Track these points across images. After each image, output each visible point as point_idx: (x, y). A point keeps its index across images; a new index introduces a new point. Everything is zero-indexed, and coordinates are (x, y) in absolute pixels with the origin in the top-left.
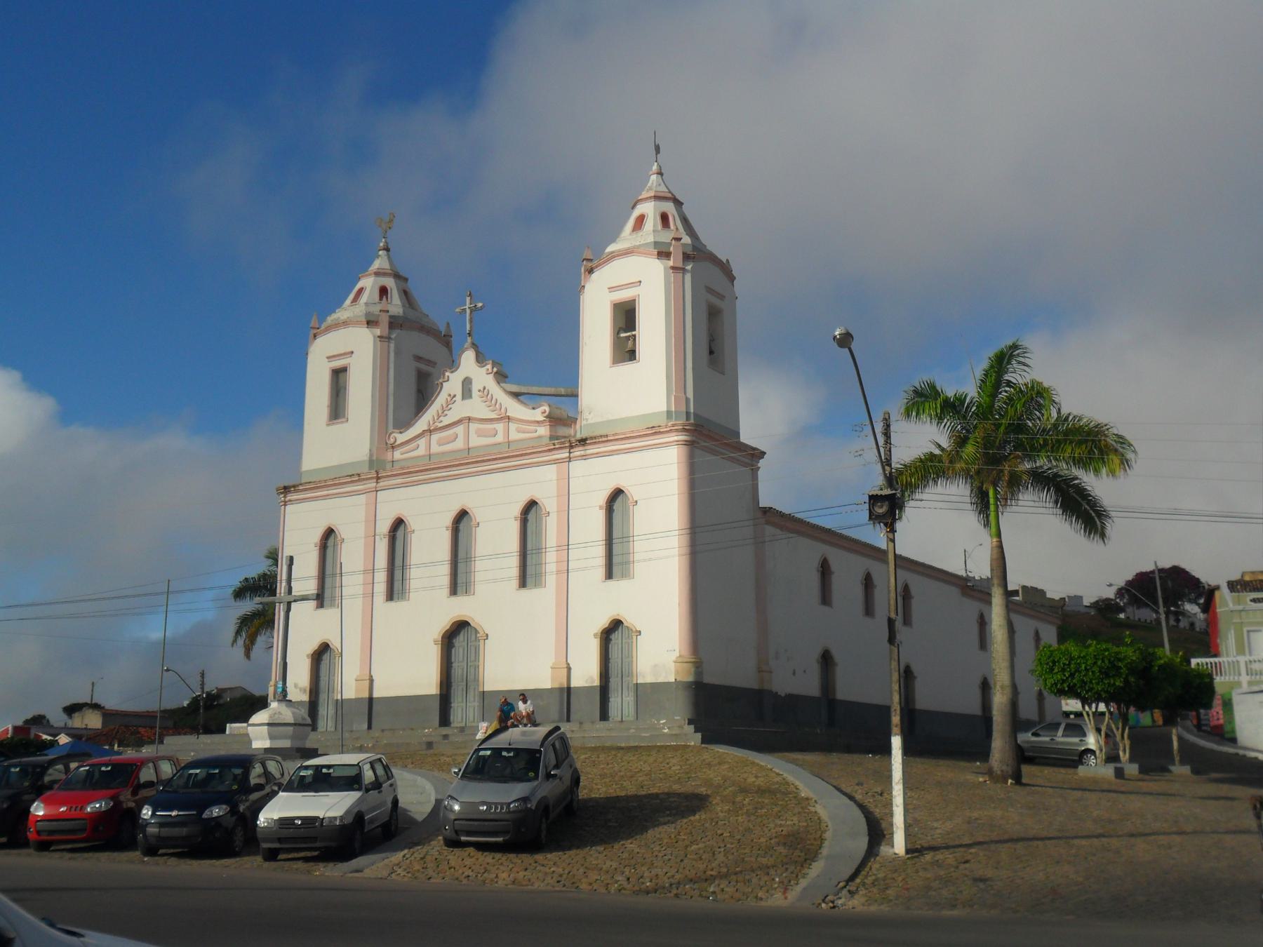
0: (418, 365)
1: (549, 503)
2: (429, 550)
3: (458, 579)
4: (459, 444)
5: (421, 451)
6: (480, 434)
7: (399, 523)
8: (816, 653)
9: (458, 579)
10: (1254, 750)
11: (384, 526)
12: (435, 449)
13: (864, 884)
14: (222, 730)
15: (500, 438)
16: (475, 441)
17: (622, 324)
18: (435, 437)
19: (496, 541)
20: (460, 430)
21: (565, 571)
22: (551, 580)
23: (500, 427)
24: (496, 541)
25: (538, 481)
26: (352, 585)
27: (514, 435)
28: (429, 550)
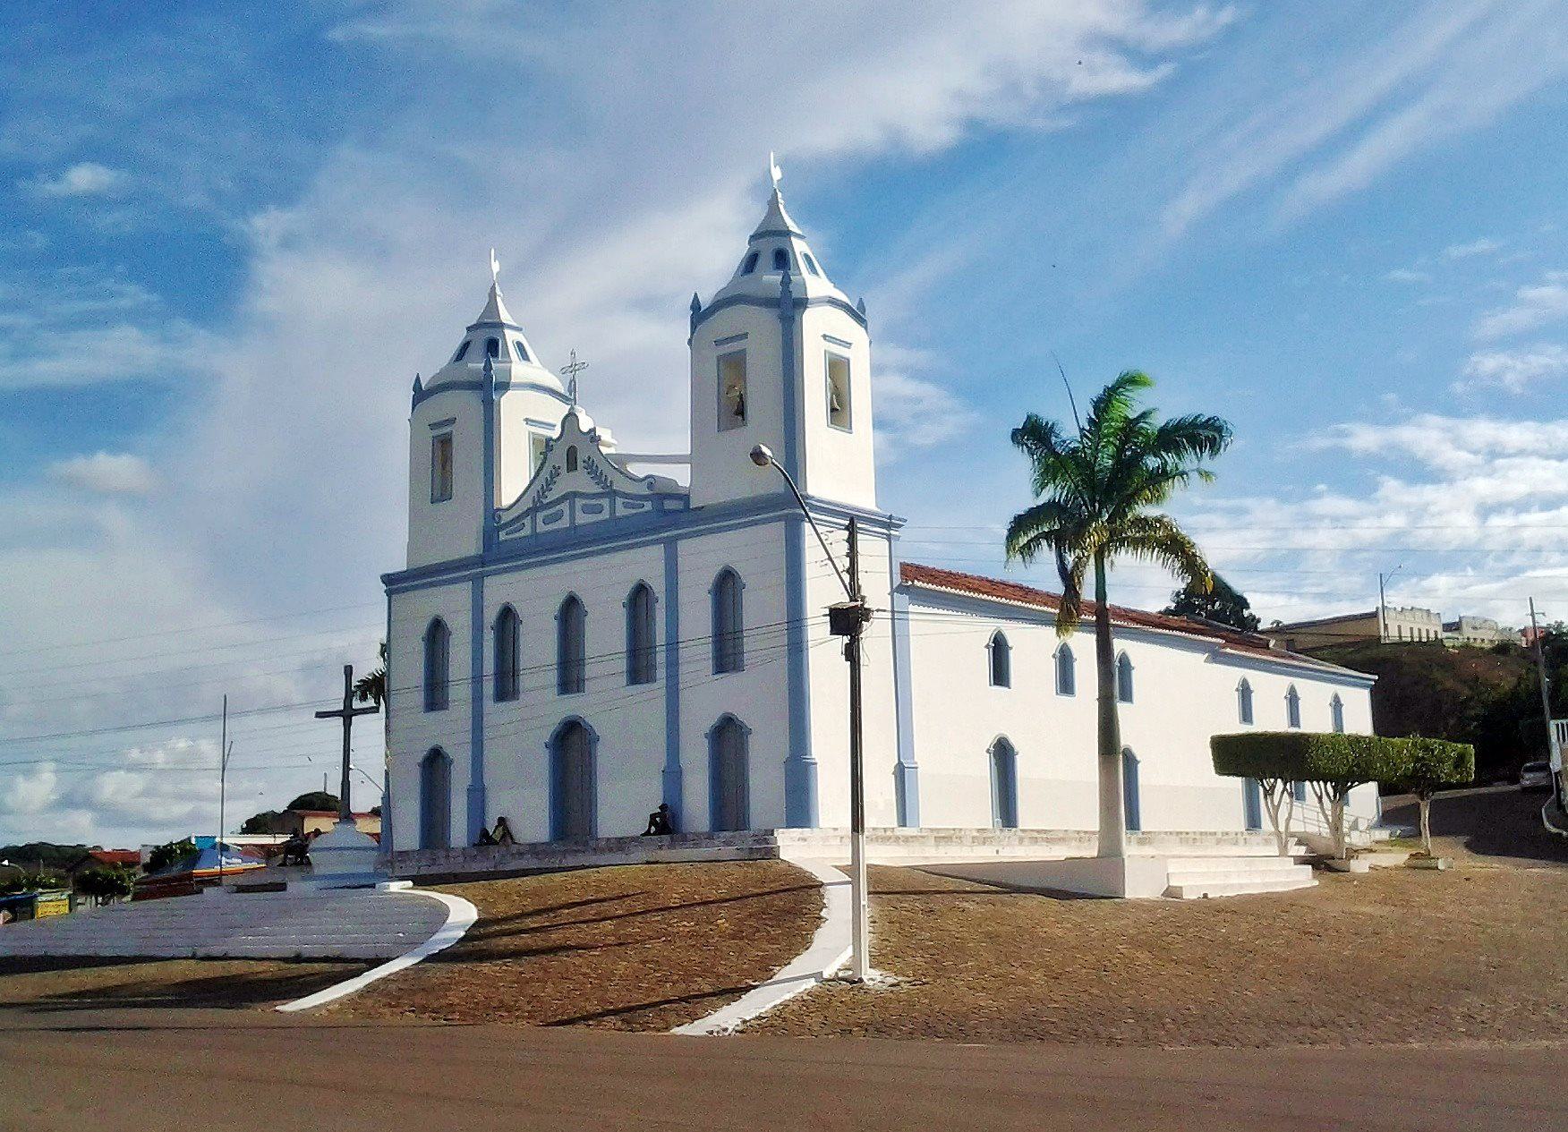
0: (533, 429)
1: (658, 587)
2: (538, 647)
3: (570, 677)
4: (564, 523)
5: (527, 531)
6: (586, 509)
7: (507, 614)
8: (989, 741)
9: (570, 677)
10: (673, 776)
11: (491, 616)
12: (542, 528)
13: (742, 950)
14: (201, 892)
15: (605, 515)
16: (582, 519)
17: (437, 494)
18: (540, 516)
19: (605, 636)
20: (565, 506)
21: (673, 665)
22: (661, 673)
23: (605, 502)
24: (605, 636)
25: (645, 563)
26: (459, 692)
27: (621, 511)
28: (538, 647)
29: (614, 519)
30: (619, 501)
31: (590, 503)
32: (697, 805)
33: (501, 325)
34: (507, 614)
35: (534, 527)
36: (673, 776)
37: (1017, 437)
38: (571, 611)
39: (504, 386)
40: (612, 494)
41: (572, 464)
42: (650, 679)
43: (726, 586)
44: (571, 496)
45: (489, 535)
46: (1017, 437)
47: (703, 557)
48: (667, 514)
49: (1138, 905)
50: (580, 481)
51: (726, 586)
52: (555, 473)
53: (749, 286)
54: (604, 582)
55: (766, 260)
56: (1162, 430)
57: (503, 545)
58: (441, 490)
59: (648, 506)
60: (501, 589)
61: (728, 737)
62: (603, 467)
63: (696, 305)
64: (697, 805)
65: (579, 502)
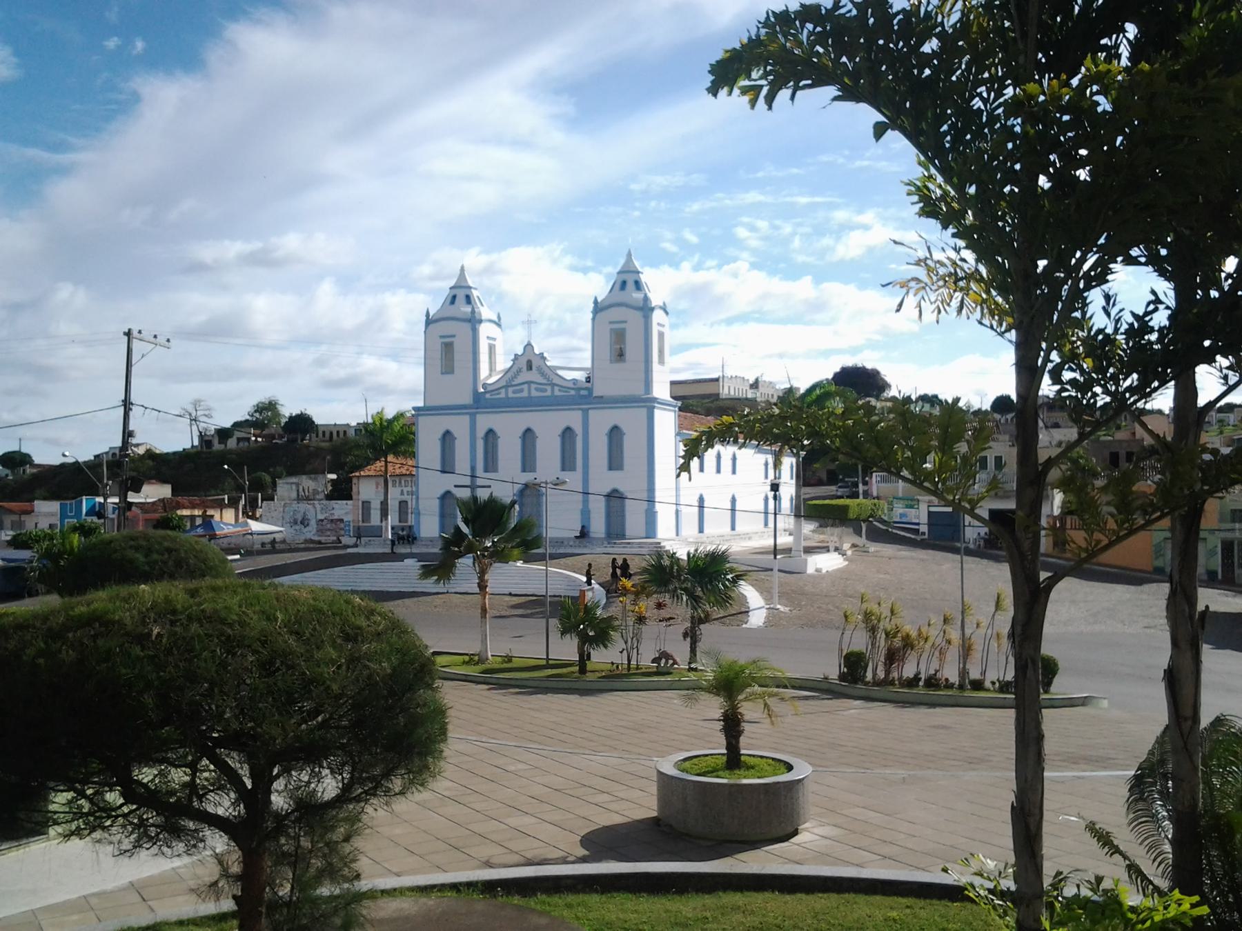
1: (578, 429)
4: (525, 394)
9: (528, 463)
10: (586, 513)
11: (481, 433)
12: (511, 395)
16: (534, 393)
18: (510, 389)
20: (525, 386)
23: (549, 388)
25: (573, 418)
27: (557, 393)
29: (530, 397)
30: (556, 388)
31: (531, 384)
32: (598, 527)
33: (470, 288)
34: (490, 432)
35: (507, 393)
36: (586, 513)
37: (125, 334)
38: (528, 436)
39: (480, 321)
40: (553, 385)
41: (530, 367)
42: (573, 469)
43: (615, 434)
44: (529, 383)
45: (477, 396)
46: (125, 334)
47: (601, 421)
48: (583, 396)
49: (809, 576)
50: (533, 376)
51: (615, 434)
52: (519, 371)
53: (621, 297)
54: (548, 426)
55: (631, 285)
56: (291, 418)
57: (482, 401)
58: (448, 367)
59: (573, 392)
60: (485, 422)
61: (615, 498)
62: (547, 371)
63: (596, 302)
64: (598, 527)
65: (533, 386)
